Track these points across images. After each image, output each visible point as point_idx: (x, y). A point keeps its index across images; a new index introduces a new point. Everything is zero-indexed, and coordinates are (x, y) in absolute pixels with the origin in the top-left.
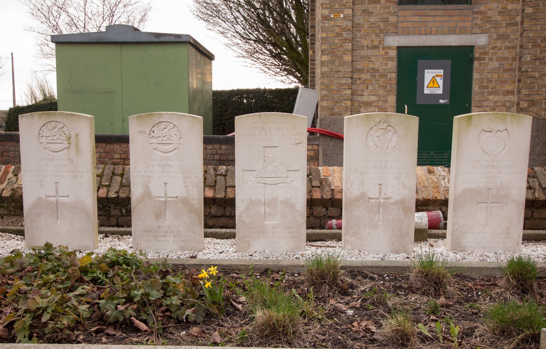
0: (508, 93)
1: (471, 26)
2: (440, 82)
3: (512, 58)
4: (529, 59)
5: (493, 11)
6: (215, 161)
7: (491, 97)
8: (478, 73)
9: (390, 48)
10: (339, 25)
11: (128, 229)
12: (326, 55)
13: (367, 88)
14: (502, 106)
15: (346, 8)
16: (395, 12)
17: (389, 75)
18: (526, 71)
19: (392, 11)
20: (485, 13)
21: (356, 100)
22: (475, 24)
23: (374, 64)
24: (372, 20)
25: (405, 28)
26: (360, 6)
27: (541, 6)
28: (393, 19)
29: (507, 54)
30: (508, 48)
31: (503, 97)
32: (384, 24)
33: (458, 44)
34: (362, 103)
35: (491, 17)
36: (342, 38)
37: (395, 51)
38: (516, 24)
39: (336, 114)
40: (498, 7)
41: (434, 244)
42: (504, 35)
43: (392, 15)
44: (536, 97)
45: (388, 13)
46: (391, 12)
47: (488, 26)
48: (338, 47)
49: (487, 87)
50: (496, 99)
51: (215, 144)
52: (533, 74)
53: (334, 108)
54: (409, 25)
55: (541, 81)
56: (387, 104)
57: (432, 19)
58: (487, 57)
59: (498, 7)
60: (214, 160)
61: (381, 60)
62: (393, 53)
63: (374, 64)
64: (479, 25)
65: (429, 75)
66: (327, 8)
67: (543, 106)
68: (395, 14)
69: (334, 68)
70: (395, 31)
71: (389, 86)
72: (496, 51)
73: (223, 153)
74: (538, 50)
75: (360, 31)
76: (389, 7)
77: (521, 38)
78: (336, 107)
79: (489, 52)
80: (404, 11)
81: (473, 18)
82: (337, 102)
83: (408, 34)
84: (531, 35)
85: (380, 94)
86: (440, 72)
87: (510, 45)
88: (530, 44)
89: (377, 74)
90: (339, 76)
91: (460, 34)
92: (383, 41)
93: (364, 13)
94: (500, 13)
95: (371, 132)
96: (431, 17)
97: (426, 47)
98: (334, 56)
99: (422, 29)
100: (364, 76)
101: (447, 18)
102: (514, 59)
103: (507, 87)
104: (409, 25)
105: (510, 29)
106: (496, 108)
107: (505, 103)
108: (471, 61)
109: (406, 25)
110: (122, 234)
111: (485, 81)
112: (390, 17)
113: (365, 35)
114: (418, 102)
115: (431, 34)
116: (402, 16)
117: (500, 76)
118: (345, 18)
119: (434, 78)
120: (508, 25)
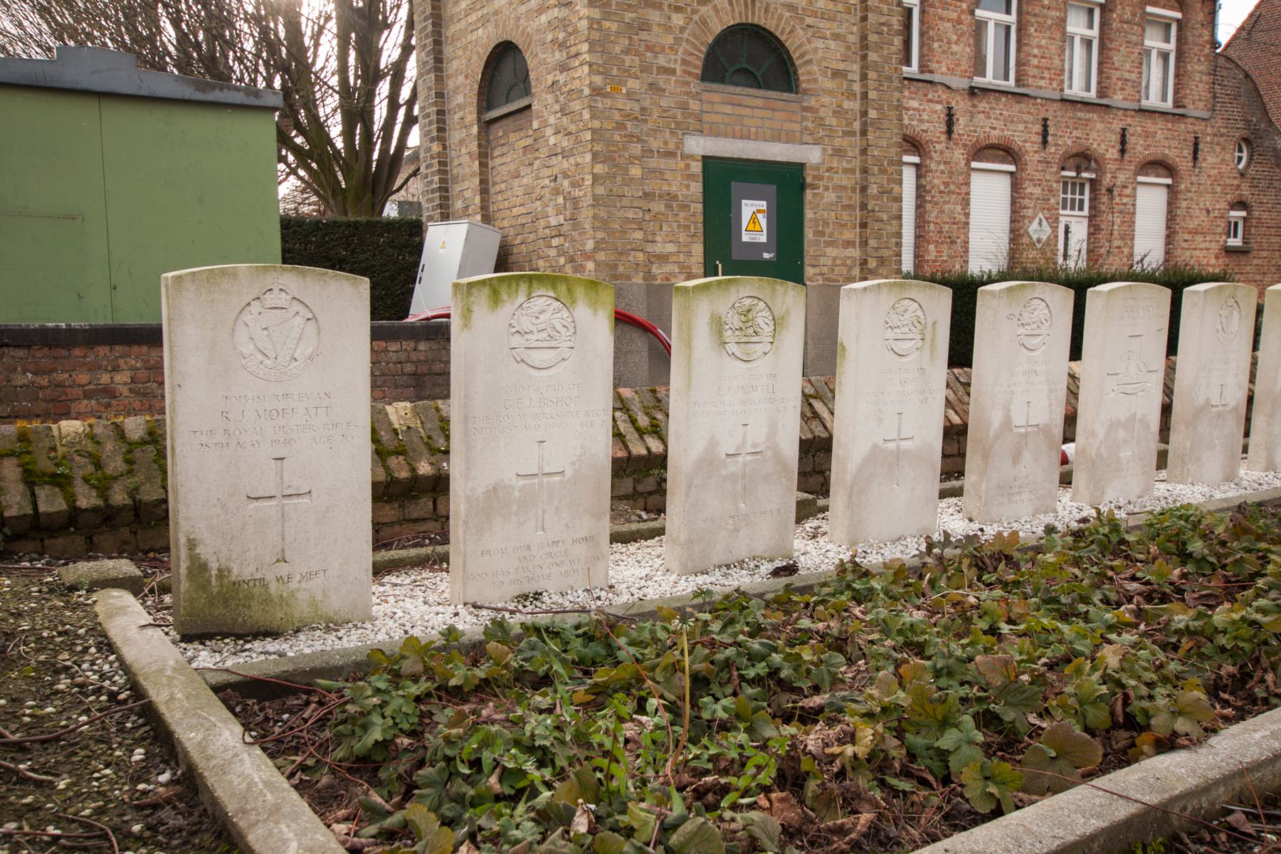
2: (763, 221)
5: (826, 109)
6: (405, 378)
7: (829, 250)
9: (691, 157)
12: (601, 162)
13: (661, 229)
15: (630, 76)
16: (697, 93)
17: (693, 205)
18: (873, 211)
24: (664, 103)
28: (694, 105)
30: (846, 171)
32: (682, 113)
34: (654, 256)
35: (822, 119)
37: (700, 164)
38: (853, 134)
41: (47, 443)
43: (693, 97)
45: (688, 93)
46: (691, 92)
50: (834, 255)
51: (405, 340)
52: (880, 214)
53: (616, 265)
54: (718, 118)
56: (691, 259)
57: (748, 112)
60: (403, 374)
62: (697, 167)
66: (600, 73)
69: (615, 189)
73: (422, 358)
74: (885, 177)
76: (688, 84)
77: (864, 158)
78: (620, 264)
80: (711, 94)
81: (802, 116)
82: (621, 254)
83: (717, 136)
84: (876, 153)
85: (681, 240)
87: (848, 166)
88: (876, 168)
89: (675, 204)
90: (623, 204)
91: (787, 142)
92: (682, 143)
93: (651, 89)
94: (834, 112)
95: (246, 317)
98: (615, 166)
101: (768, 113)
102: (853, 190)
104: (718, 118)
108: (802, 187)
109: (714, 118)
112: (691, 101)
113: (655, 131)
114: (736, 255)
115: (749, 138)
116: (709, 102)
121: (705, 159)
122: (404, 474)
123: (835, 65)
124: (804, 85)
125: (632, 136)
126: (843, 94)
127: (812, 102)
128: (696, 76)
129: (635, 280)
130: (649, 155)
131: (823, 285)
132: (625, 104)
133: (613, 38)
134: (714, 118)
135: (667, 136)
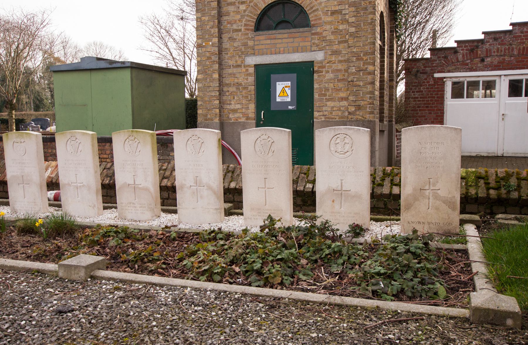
0: (342, 99)
1: (310, 45)
2: (289, 92)
3: (344, 70)
4: (354, 70)
5: (327, 32)
8: (317, 83)
9: (249, 66)
10: (209, 50)
11: (114, 205)
12: (201, 74)
13: (234, 98)
14: (337, 110)
15: (213, 37)
16: (252, 37)
17: (249, 87)
19: (250, 36)
20: (321, 33)
21: (226, 108)
22: (314, 44)
23: (238, 79)
24: (236, 44)
25: (260, 49)
26: (227, 34)
27: (362, 25)
28: (251, 43)
29: (340, 67)
30: (340, 61)
31: (339, 103)
33: (300, 60)
34: (230, 110)
35: (326, 37)
36: (211, 60)
37: (253, 68)
39: (209, 119)
40: (331, 28)
42: (337, 51)
44: (361, 103)
45: (247, 39)
46: (249, 37)
47: (324, 44)
48: (208, 68)
49: (325, 95)
50: (332, 105)
52: (358, 83)
54: (263, 47)
55: (365, 89)
57: (280, 41)
58: (324, 70)
59: (331, 28)
61: (243, 76)
62: (252, 70)
63: (238, 79)
64: (316, 44)
65: (280, 86)
66: (201, 38)
67: (368, 110)
68: (252, 39)
69: (206, 84)
70: (253, 52)
71: (249, 96)
72: (331, 65)
74: (362, 63)
75: (227, 54)
79: (325, 66)
82: (209, 110)
83: (263, 54)
84: (355, 50)
85: (243, 102)
86: (288, 84)
87: (342, 59)
88: (355, 58)
89: (241, 87)
91: (302, 52)
93: (229, 40)
96: (279, 40)
97: (277, 64)
98: (206, 75)
99: (272, 49)
100: (232, 89)
101: (291, 40)
103: (342, 95)
104: (263, 47)
105: (342, 46)
106: (333, 112)
107: (340, 108)
109: (261, 47)
110: (111, 208)
111: (324, 89)
112: (249, 42)
114: (273, 108)
115: (280, 53)
117: (335, 85)
118: (213, 45)
119: (283, 89)
120: (340, 43)
121: (256, 66)
122: (504, 196)
123: (333, 8)
124: (312, 23)
125: (214, 61)
126: (338, 22)
127: (319, 30)
128: (252, 30)
129: (215, 121)
130: (229, 68)
131: (324, 121)
132: (211, 49)
133: (206, 23)
134: (261, 47)
135: (237, 58)
